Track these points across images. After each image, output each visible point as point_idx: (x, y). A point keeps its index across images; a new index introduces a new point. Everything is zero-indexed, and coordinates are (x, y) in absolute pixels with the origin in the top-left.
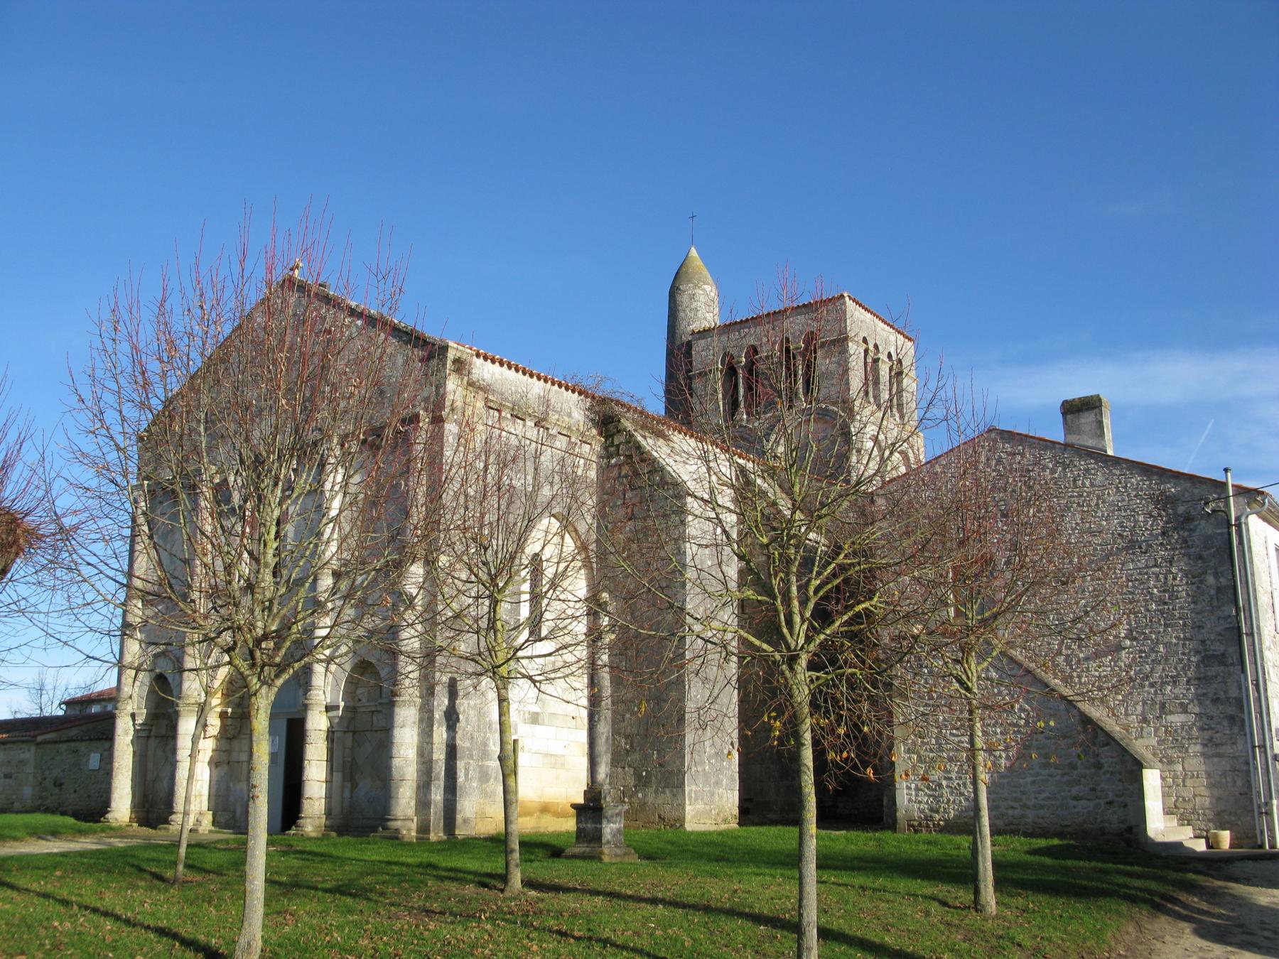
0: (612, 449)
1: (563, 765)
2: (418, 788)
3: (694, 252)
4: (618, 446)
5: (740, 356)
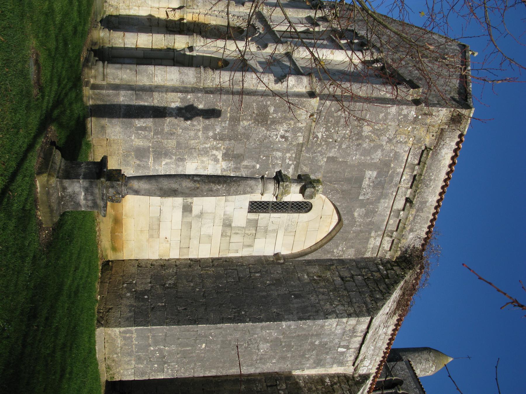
0: (389, 266)
1: (151, 236)
2: (129, 85)
3: (450, 359)
4: (392, 269)
5: (402, 389)
